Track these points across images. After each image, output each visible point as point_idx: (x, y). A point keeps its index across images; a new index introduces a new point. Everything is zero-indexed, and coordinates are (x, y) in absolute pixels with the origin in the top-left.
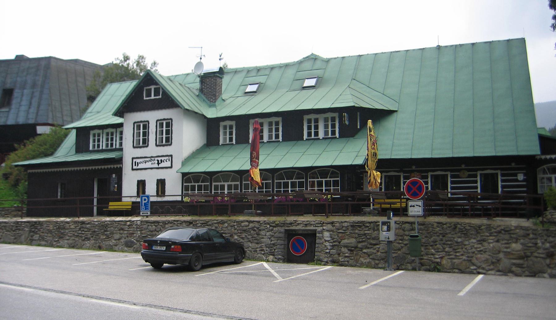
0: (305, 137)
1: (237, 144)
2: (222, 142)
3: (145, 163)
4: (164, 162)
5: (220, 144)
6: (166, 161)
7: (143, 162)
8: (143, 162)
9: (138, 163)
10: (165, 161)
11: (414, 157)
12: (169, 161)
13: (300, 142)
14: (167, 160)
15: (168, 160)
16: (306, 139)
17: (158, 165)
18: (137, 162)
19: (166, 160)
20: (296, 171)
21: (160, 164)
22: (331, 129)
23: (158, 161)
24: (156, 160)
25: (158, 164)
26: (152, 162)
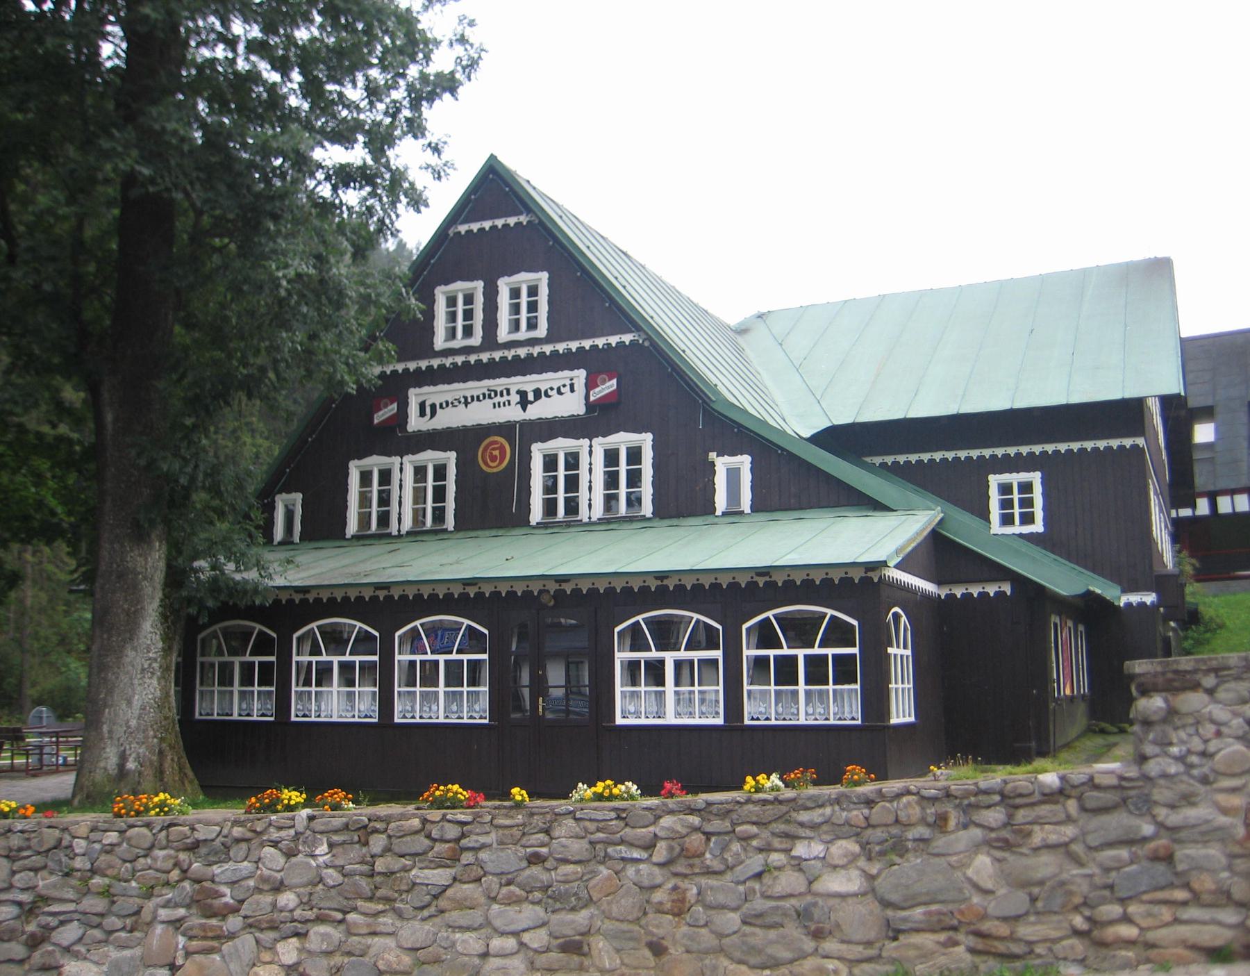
0: (536, 514)
1: (662, 518)
2: (602, 512)
3: (466, 404)
4: (547, 395)
5: (348, 536)
6: (559, 392)
7: (456, 403)
8: (456, 403)
9: (433, 407)
10: (555, 391)
11: (1076, 399)
12: (572, 390)
13: (710, 519)
14: (563, 390)
15: (568, 387)
16: (724, 514)
17: (524, 409)
18: (428, 403)
19: (559, 389)
20: (820, 647)
21: (531, 403)
22: (1033, 512)
23: (523, 394)
24: (513, 391)
25: (524, 403)
26: (498, 399)
